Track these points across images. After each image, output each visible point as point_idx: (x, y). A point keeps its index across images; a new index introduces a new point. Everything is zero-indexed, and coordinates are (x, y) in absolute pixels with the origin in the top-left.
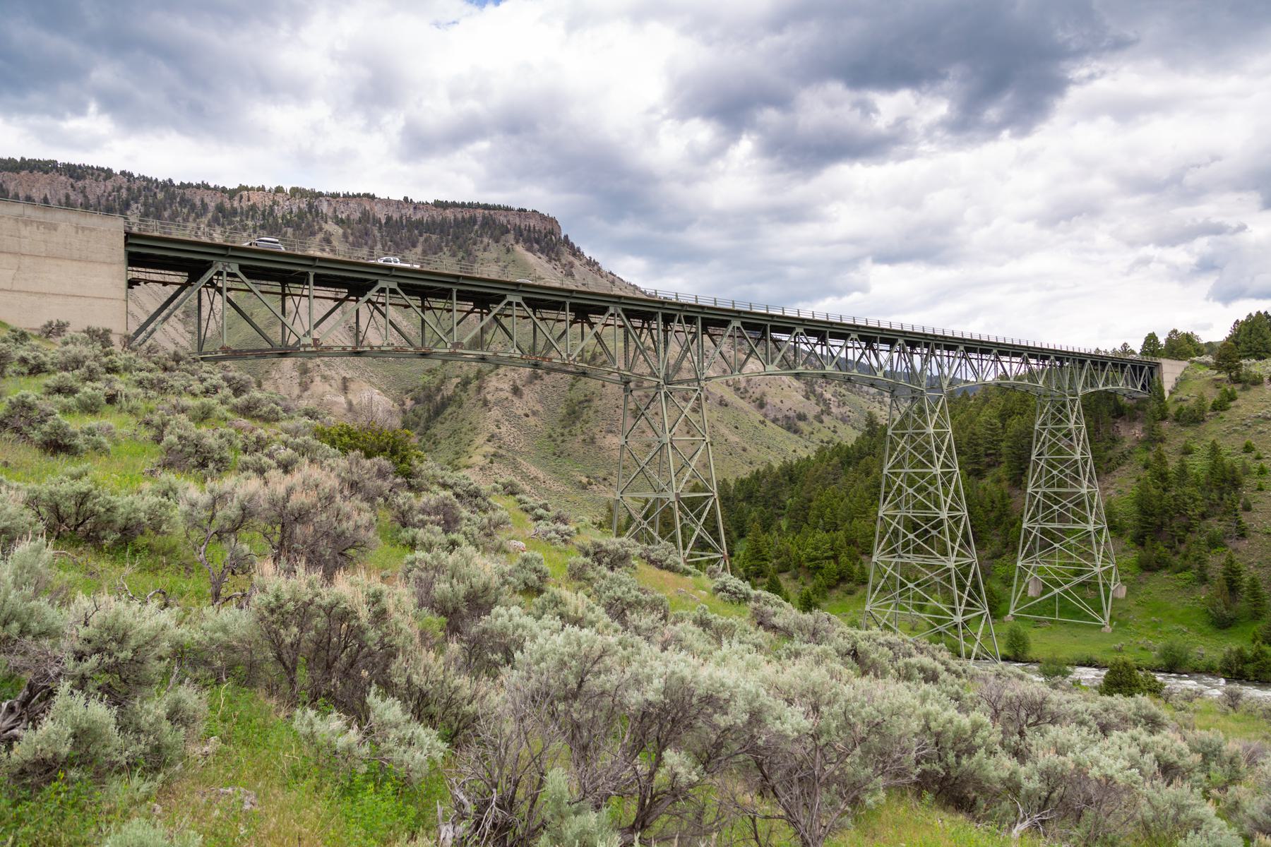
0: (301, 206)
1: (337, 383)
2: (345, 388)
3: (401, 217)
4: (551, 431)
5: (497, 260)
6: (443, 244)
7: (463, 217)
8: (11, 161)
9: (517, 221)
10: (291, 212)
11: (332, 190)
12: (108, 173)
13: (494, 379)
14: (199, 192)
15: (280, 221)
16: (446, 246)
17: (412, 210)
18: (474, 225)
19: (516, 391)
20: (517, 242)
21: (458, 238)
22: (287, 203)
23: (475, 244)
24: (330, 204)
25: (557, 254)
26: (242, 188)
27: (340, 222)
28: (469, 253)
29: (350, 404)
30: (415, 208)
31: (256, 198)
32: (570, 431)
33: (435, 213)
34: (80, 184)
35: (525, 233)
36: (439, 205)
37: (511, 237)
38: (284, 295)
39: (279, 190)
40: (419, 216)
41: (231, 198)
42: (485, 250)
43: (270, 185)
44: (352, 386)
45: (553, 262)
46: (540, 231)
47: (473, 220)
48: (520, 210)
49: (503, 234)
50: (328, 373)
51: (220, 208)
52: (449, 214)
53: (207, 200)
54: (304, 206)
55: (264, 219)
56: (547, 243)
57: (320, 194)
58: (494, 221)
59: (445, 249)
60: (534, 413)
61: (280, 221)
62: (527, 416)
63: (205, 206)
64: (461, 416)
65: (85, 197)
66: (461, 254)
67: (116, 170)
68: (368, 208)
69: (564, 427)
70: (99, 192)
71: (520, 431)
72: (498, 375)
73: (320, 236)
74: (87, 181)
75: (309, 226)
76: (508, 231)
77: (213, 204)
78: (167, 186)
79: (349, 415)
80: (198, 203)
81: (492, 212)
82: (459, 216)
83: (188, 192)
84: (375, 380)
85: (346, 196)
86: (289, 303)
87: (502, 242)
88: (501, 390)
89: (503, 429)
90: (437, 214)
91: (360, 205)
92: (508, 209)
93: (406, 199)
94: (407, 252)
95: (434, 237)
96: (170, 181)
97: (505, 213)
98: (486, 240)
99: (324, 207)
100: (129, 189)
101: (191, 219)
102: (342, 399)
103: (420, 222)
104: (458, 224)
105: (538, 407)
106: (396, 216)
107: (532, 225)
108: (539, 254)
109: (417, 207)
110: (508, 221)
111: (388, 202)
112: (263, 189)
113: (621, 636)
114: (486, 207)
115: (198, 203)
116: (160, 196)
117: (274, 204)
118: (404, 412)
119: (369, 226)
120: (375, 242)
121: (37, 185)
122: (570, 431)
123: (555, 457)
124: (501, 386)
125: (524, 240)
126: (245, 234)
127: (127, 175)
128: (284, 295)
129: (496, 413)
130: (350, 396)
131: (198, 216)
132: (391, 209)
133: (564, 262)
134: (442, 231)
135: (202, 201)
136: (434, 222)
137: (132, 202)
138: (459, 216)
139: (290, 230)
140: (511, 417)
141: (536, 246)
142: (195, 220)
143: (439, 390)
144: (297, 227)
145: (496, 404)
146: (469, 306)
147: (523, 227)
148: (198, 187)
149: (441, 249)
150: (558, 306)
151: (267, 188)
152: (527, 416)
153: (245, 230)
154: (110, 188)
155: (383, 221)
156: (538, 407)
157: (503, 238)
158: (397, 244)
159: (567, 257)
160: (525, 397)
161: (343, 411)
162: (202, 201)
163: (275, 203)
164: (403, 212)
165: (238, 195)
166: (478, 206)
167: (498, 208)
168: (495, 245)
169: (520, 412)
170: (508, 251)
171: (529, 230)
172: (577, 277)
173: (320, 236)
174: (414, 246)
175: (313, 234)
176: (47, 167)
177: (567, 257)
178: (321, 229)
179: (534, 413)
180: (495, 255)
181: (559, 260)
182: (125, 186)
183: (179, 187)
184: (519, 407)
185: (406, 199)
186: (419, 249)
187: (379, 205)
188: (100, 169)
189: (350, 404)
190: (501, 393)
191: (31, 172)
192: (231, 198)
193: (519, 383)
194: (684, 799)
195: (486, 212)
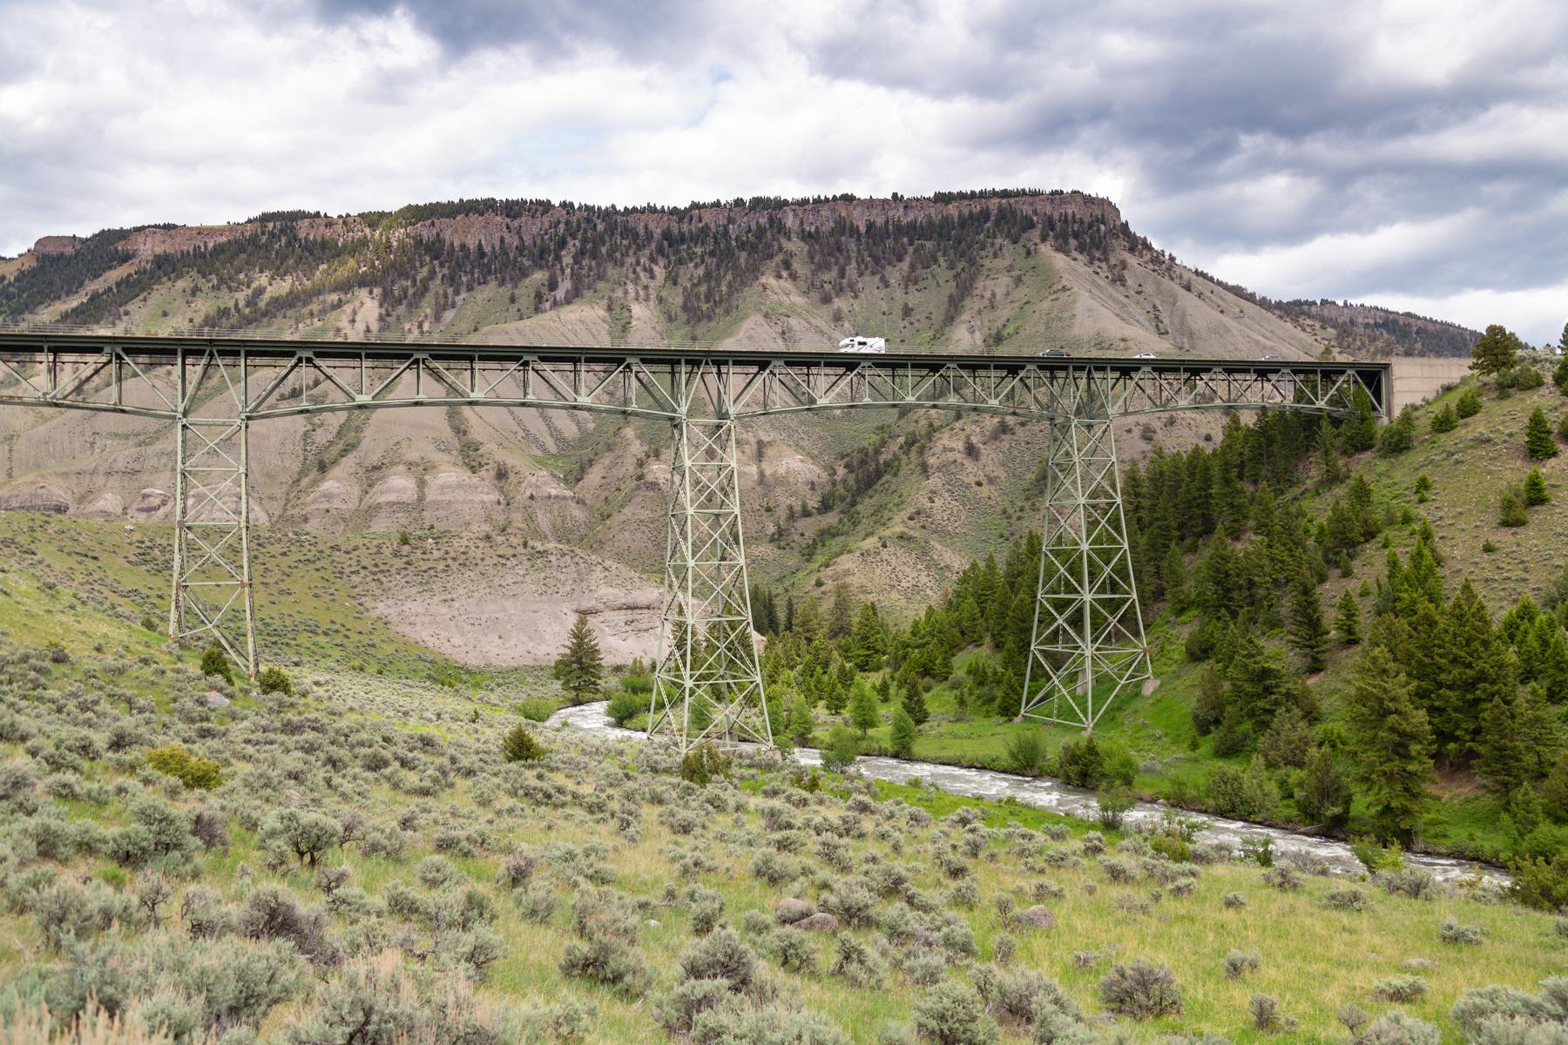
0: (761, 220)
1: (751, 449)
2: (760, 455)
3: (887, 222)
4: (1008, 505)
5: (1010, 269)
6: (939, 254)
7: (970, 212)
8: (451, 204)
9: (1048, 210)
10: (750, 231)
11: (799, 196)
12: (546, 206)
13: (946, 435)
14: (643, 217)
15: (734, 243)
16: (944, 255)
17: (901, 210)
18: (986, 222)
19: (971, 451)
20: (1044, 240)
21: (960, 243)
22: (745, 219)
23: (983, 248)
24: (796, 215)
25: (1105, 252)
26: (695, 206)
27: (806, 237)
28: (972, 262)
29: (762, 474)
30: (906, 207)
31: (707, 217)
32: (1033, 505)
33: (932, 211)
34: (516, 223)
35: (1058, 226)
36: (942, 199)
37: (1035, 234)
38: (894, 376)
39: (739, 202)
40: (911, 217)
41: (681, 220)
42: (995, 256)
43: (726, 197)
44: (769, 452)
45: (1096, 262)
46: (1082, 222)
47: (985, 215)
48: (1054, 193)
49: (1024, 230)
50: (745, 436)
51: (667, 235)
52: (952, 210)
53: (652, 226)
54: (763, 221)
55: (716, 242)
56: (1092, 238)
57: (786, 203)
58: (1013, 213)
59: (941, 260)
60: (991, 481)
61: (734, 243)
62: (979, 484)
63: (649, 235)
64: (893, 487)
65: (521, 238)
66: (962, 264)
67: (556, 202)
68: (844, 214)
69: (1028, 499)
70: (535, 230)
71: (964, 505)
72: (952, 429)
73: (779, 258)
74: (523, 219)
75: (768, 246)
76: (1032, 225)
77: (659, 231)
78: (612, 212)
79: (759, 489)
80: (641, 231)
81: (1012, 201)
82: (966, 212)
83: (631, 219)
84: (805, 443)
85: (817, 201)
86: (897, 379)
87: (1022, 242)
88: (952, 450)
89: (938, 502)
90: (934, 212)
91: (833, 211)
92: (1035, 194)
93: (895, 195)
94: (889, 269)
95: (929, 244)
96: (613, 206)
97: (1030, 199)
98: (999, 241)
99: (790, 221)
100: (567, 223)
101: (631, 252)
102: (754, 469)
103: (912, 226)
104: (964, 222)
105: (1001, 473)
106: (880, 221)
107: (1070, 212)
108: (1075, 254)
109: (908, 204)
110: (1035, 212)
111: (871, 203)
112: (717, 204)
113: (44, 988)
114: (1005, 194)
115: (641, 231)
116: (600, 227)
117: (729, 222)
118: (834, 483)
119: (843, 239)
120: (849, 258)
121: (473, 230)
122: (1033, 505)
123: (1001, 540)
124: (953, 445)
125: (1056, 238)
126: (691, 265)
127: (566, 206)
128: (894, 376)
129: (935, 481)
130: (764, 465)
131: (639, 248)
132: (875, 212)
133: (1113, 261)
134: (940, 235)
135: (646, 227)
136: (931, 223)
137: (569, 239)
138: (966, 212)
139: (744, 255)
140: (956, 487)
141: (1073, 242)
142: (635, 253)
143: (877, 452)
144: (754, 248)
145: (939, 469)
146: (1117, 375)
147: (1056, 216)
148: (643, 211)
149: (936, 260)
150: (1247, 371)
151: (723, 202)
152: (979, 484)
153: (691, 260)
154: (547, 225)
155: (863, 229)
156: (1001, 473)
157: (1025, 235)
158: (876, 261)
159: (1120, 253)
160: (983, 459)
161: (751, 484)
162: (646, 227)
163: (731, 221)
164: (890, 214)
165: (688, 217)
166: (994, 194)
167: (1021, 194)
168: (1011, 247)
169: (971, 480)
170: (1028, 253)
171: (1066, 221)
172: (1130, 282)
173: (779, 258)
174: (900, 260)
175: (771, 256)
176: (489, 205)
177: (1120, 253)
178: (781, 249)
179: (991, 481)
180: (1007, 262)
181: (1106, 260)
182: (563, 220)
183: (623, 214)
184: (971, 471)
185: (895, 195)
186: (905, 265)
187: (859, 209)
188: (539, 203)
189: (762, 474)
190: (950, 454)
191: (467, 215)
192: (681, 220)
193: (974, 440)
194: (1355, 988)
195: (1004, 201)
